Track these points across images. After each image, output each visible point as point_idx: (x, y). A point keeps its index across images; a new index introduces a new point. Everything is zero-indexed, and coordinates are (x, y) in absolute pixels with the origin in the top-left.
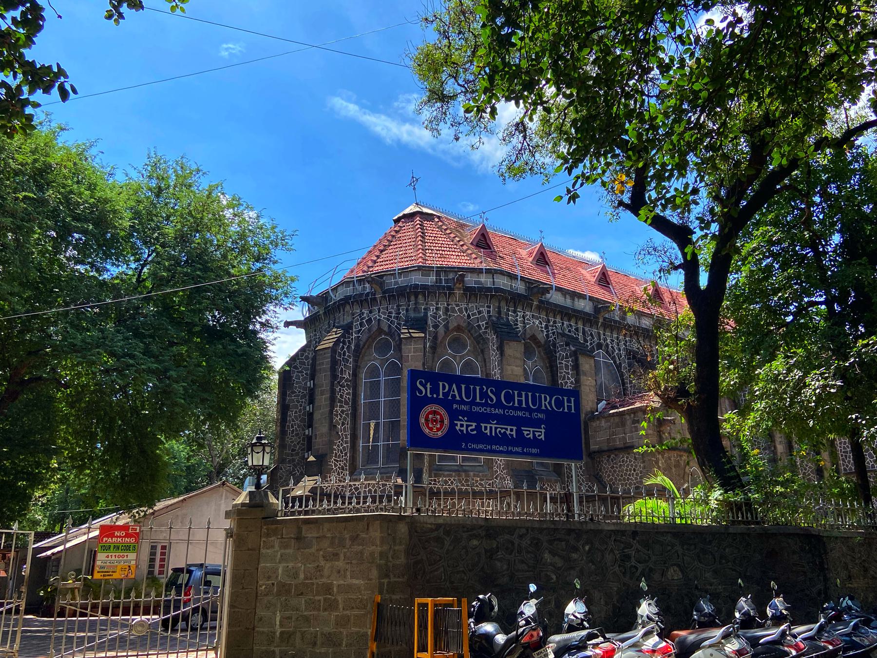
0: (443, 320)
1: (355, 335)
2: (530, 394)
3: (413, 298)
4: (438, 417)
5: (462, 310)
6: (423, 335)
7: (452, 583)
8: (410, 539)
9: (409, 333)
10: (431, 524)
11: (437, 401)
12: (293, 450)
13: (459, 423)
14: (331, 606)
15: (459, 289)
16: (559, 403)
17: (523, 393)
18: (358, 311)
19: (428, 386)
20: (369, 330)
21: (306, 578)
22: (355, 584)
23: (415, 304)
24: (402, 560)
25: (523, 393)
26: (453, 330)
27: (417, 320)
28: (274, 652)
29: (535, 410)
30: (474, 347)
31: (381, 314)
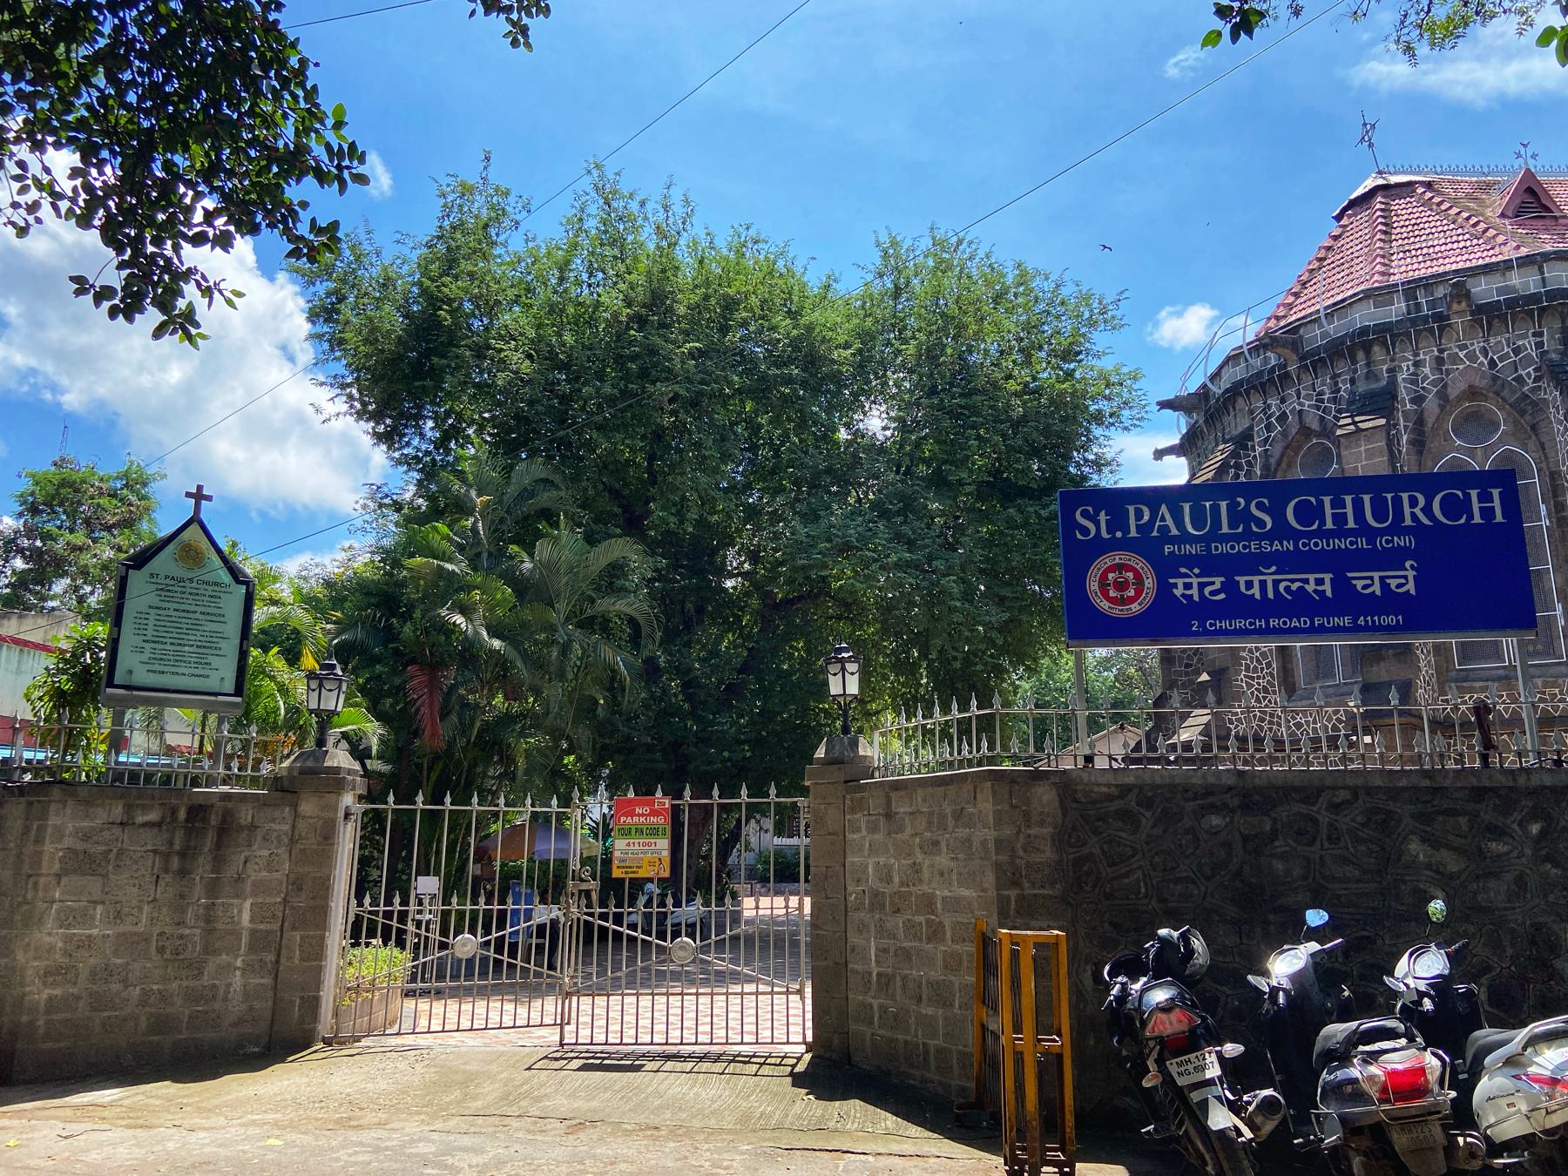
0: (1434, 384)
1: (1259, 449)
2: (1367, 498)
3: (1361, 355)
4: (1130, 575)
5: (1471, 355)
6: (1383, 421)
7: (1162, 900)
8: (1064, 815)
9: (1354, 423)
10: (1109, 785)
11: (1126, 545)
12: (1187, 666)
13: (1180, 582)
14: (936, 933)
15: (1460, 313)
16: (1455, 507)
17: (1348, 499)
18: (1260, 404)
19: (1103, 517)
20: (1284, 434)
21: (902, 884)
22: (965, 898)
23: (1368, 365)
24: (1048, 854)
25: (1348, 499)
26: (1460, 399)
27: (1371, 396)
28: (871, 1005)
29: (1382, 532)
30: (1516, 423)
31: (1302, 401)
